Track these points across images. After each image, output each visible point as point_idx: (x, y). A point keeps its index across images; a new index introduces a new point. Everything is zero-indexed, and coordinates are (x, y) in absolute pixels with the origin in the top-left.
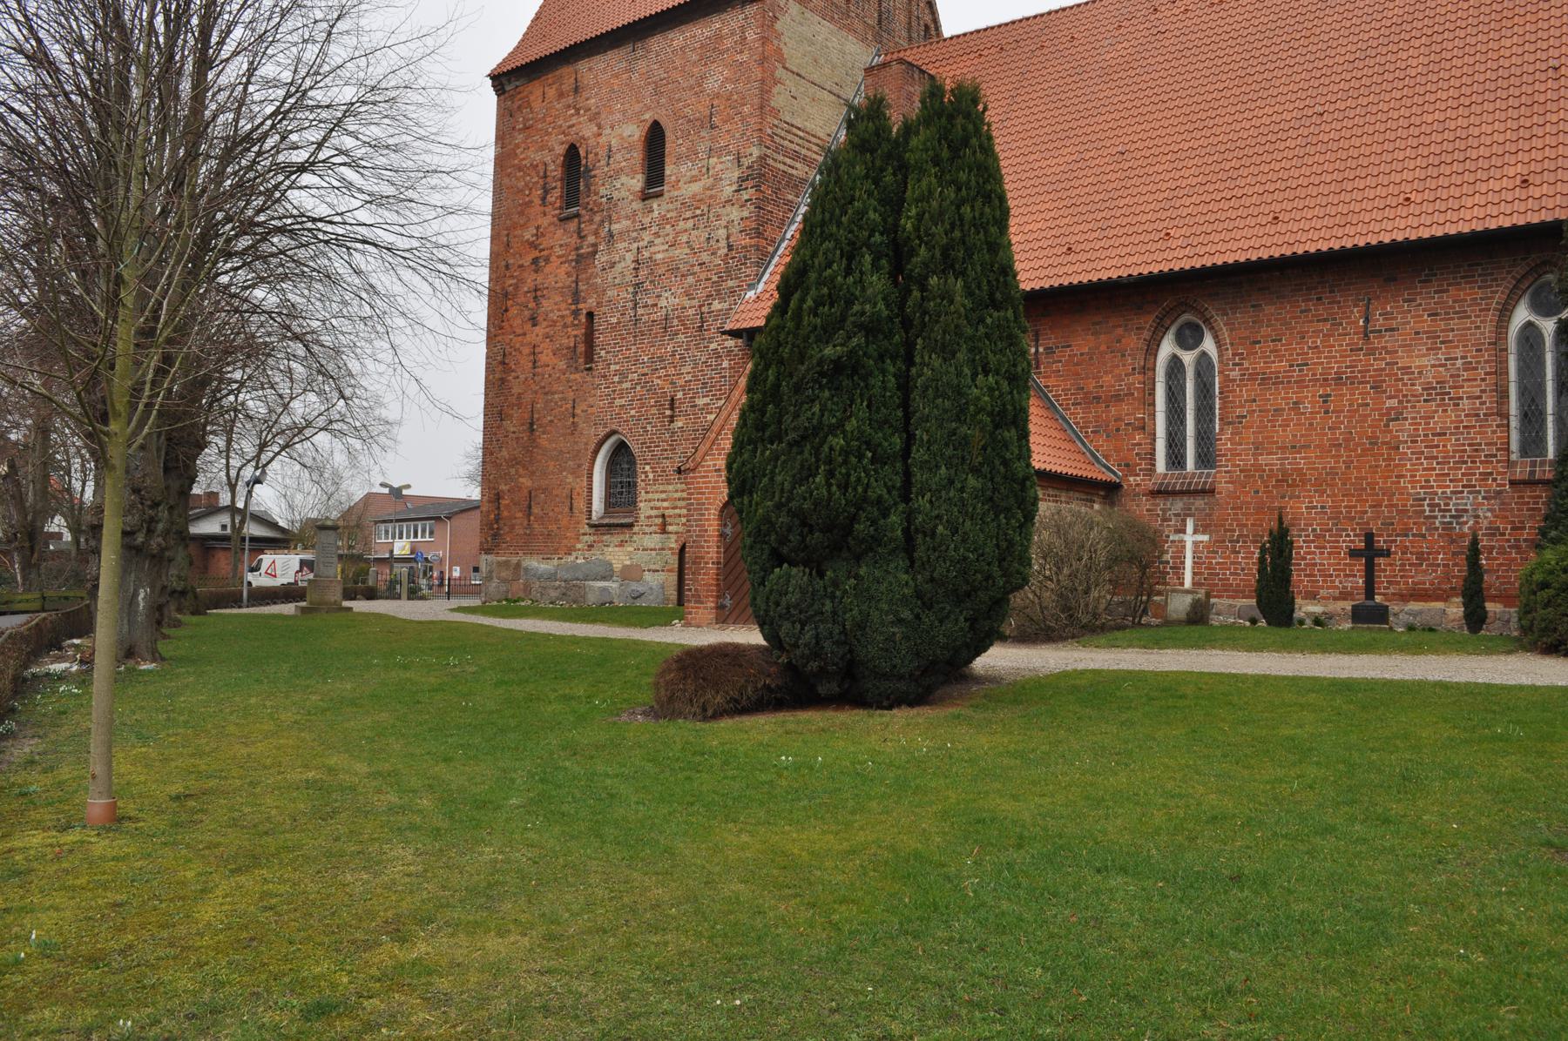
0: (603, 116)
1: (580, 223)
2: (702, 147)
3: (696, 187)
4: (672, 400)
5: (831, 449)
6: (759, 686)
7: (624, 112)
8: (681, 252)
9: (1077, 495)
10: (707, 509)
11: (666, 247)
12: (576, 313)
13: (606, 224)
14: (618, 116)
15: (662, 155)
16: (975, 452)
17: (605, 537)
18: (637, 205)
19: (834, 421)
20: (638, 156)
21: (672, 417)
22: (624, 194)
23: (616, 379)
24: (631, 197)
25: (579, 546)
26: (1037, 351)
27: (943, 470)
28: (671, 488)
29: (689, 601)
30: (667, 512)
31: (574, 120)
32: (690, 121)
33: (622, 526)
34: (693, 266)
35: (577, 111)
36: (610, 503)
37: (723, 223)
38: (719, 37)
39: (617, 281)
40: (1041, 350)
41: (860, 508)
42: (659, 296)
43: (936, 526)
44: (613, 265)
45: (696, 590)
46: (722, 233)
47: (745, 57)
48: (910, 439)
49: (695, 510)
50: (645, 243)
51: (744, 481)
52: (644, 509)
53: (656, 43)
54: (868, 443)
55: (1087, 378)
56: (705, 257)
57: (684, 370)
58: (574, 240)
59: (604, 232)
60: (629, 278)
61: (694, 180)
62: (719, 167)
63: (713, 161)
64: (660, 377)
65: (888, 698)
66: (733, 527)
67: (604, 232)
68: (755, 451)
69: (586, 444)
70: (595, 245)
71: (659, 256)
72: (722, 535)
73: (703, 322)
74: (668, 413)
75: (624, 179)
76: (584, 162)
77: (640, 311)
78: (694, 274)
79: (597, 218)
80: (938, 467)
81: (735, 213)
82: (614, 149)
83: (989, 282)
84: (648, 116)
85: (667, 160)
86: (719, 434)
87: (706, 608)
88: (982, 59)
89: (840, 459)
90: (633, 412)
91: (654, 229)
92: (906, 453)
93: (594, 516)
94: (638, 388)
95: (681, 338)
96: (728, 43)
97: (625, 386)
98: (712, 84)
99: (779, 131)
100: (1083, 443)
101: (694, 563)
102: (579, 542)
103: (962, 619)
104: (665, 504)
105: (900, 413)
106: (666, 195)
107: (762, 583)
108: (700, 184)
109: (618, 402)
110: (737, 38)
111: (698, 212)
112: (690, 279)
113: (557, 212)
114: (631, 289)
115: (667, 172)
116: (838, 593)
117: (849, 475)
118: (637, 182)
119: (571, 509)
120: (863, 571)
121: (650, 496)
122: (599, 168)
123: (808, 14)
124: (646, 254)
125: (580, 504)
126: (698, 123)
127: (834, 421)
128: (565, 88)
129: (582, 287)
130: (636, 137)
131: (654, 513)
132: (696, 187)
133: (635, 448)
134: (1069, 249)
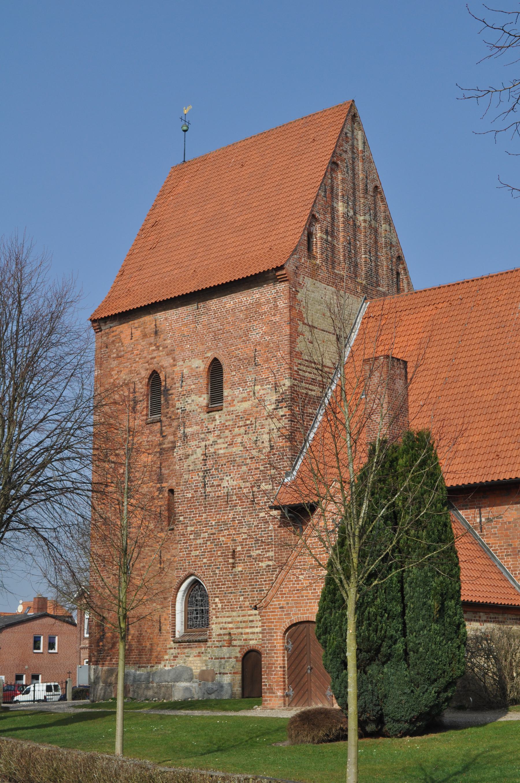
0: (177, 353)
1: (161, 426)
2: (250, 378)
3: (246, 405)
4: (234, 551)
5: (369, 613)
6: (338, 728)
7: (192, 351)
8: (237, 449)
9: (510, 616)
10: (275, 633)
11: (226, 445)
12: (160, 490)
13: (182, 428)
14: (188, 353)
15: (221, 382)
16: (435, 613)
17: (186, 650)
18: (206, 416)
19: (369, 600)
20: (203, 381)
21: (233, 564)
22: (194, 407)
23: (192, 537)
24: (199, 410)
25: (166, 657)
26: (481, 521)
27: (421, 622)
28: (234, 614)
29: (266, 693)
30: (232, 631)
31: (155, 354)
32: (240, 360)
33: (199, 641)
34: (246, 459)
35: (158, 347)
36: (189, 624)
37: (266, 430)
38: (258, 304)
39: (191, 468)
40: (483, 520)
41: (383, 641)
42: (222, 479)
43: (419, 648)
44: (187, 456)
45: (270, 685)
46: (266, 437)
47: (277, 318)
48: (404, 607)
49: (267, 633)
50: (211, 442)
51: (326, 628)
52: (215, 629)
53: (214, 304)
54: (385, 610)
55: (514, 539)
56: (254, 453)
57: (242, 530)
58: (157, 439)
59: (180, 434)
60: (199, 466)
61: (244, 400)
62: (262, 392)
63: (258, 388)
64: (224, 536)
65: (400, 733)
66: (293, 644)
67: (180, 434)
68: (331, 613)
69: (171, 583)
70: (174, 442)
71: (221, 451)
72: (286, 649)
73: (254, 498)
74: (231, 561)
75: (193, 397)
76: (163, 384)
77: (208, 489)
78: (248, 464)
79: (175, 424)
80: (419, 620)
81: (274, 424)
82: (186, 376)
83: (438, 530)
84: (210, 355)
85: (225, 385)
86: (281, 584)
87: (276, 697)
88: (439, 311)
89: (374, 618)
90: (205, 560)
91: (217, 433)
92: (403, 614)
93: (177, 636)
94: (209, 543)
95: (239, 509)
96: (265, 308)
97: (198, 541)
98: (255, 336)
99: (301, 367)
100: (514, 581)
101: (268, 668)
102: (167, 654)
103: (433, 692)
104: (231, 626)
105: (399, 594)
106: (225, 410)
107: (337, 677)
108: (250, 403)
109: (193, 553)
110: (271, 305)
111: (248, 422)
112: (244, 468)
113: (145, 418)
114: (201, 474)
115: (225, 394)
116: (374, 681)
117: (377, 625)
118: (203, 400)
119: (160, 630)
120: (385, 670)
121: (220, 620)
122: (175, 388)
123: (318, 284)
124: (212, 450)
125: (167, 627)
126: (246, 362)
127: (369, 600)
128: (148, 331)
129: (164, 471)
130: (201, 369)
131: (222, 632)
132: (246, 405)
133: (207, 586)
134: (498, 456)
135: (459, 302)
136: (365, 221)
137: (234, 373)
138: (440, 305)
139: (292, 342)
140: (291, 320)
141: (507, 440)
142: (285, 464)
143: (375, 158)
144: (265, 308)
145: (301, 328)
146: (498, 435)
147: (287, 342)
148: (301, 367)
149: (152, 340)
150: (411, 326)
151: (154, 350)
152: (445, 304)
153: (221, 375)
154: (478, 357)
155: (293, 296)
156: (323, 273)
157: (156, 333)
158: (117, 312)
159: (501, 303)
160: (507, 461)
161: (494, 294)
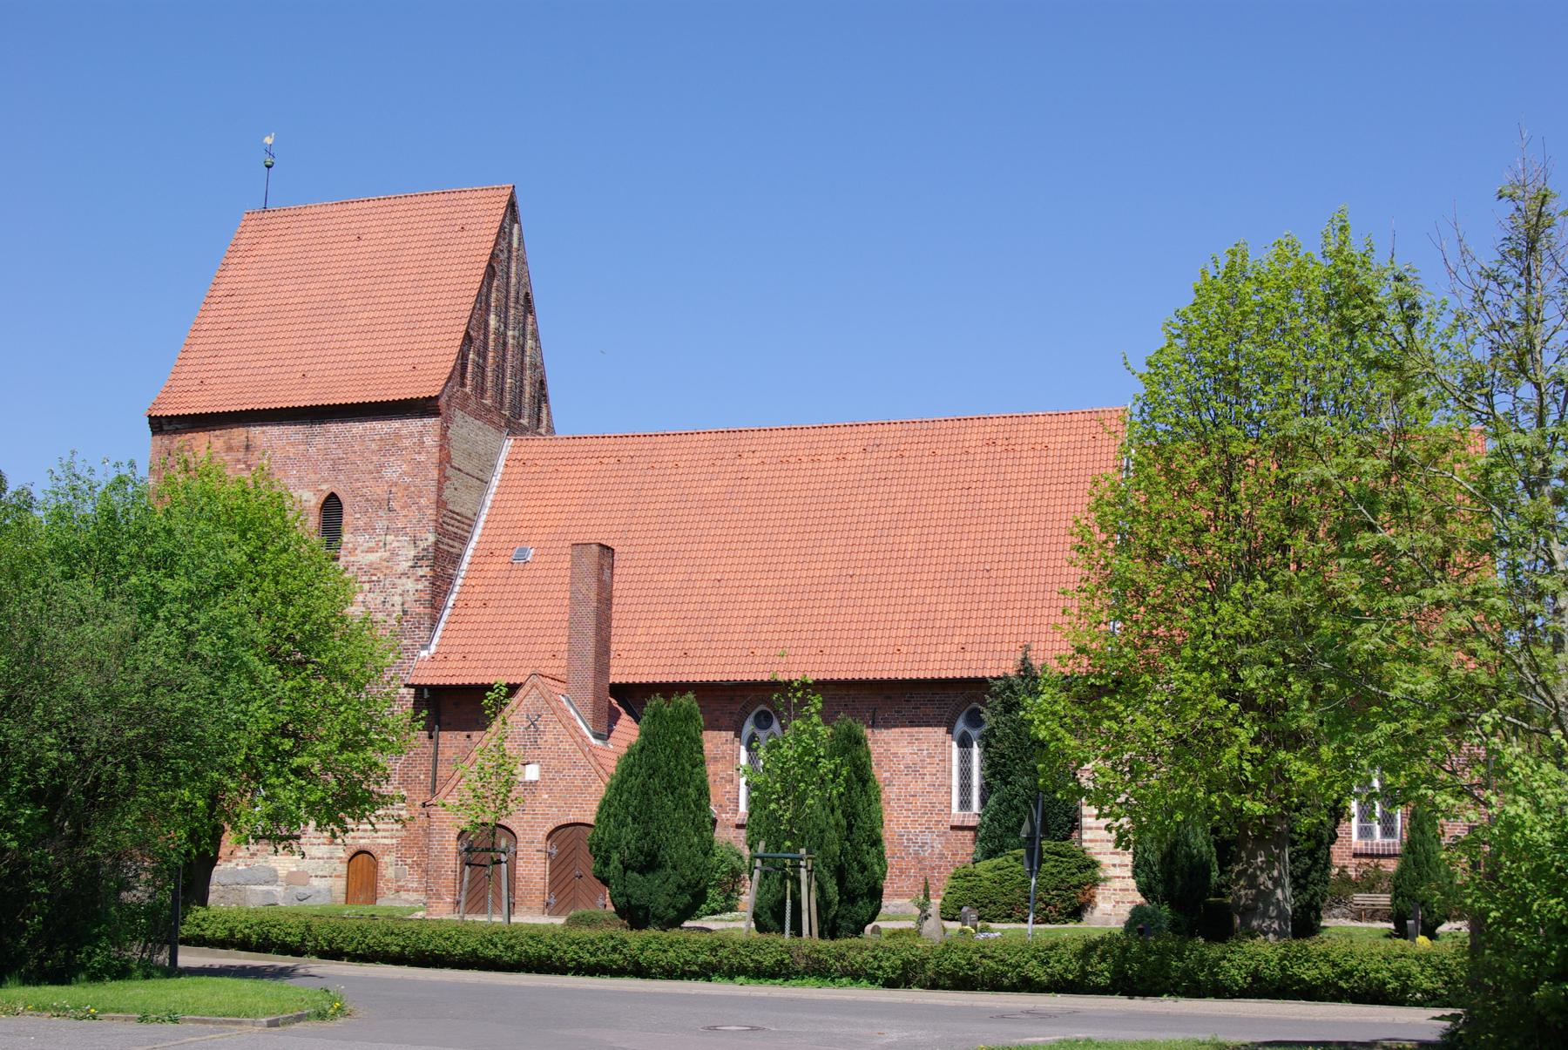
2: (380, 524)
7: (300, 479)
32: (367, 500)
38: (398, 435)
46: (397, 600)
47: (423, 458)
53: (334, 428)
61: (370, 550)
62: (395, 544)
63: (390, 538)
84: (326, 488)
88: (604, 467)
98: (390, 474)
99: (446, 519)
111: (374, 578)
126: (377, 504)
135: (629, 460)
136: (514, 337)
137: (358, 516)
138: (606, 461)
139: (440, 489)
140: (441, 463)
141: (696, 637)
142: (422, 634)
143: (529, 260)
144: (407, 443)
145: (449, 472)
146: (685, 630)
147: (433, 489)
148: (446, 519)
149: (241, 455)
150: (570, 481)
151: (243, 470)
152: (612, 460)
153: (340, 514)
154: (299, 334)
155: (445, 430)
156: (472, 404)
157: (247, 448)
158: (192, 412)
159: (680, 471)
160: (696, 661)
161: (672, 458)
